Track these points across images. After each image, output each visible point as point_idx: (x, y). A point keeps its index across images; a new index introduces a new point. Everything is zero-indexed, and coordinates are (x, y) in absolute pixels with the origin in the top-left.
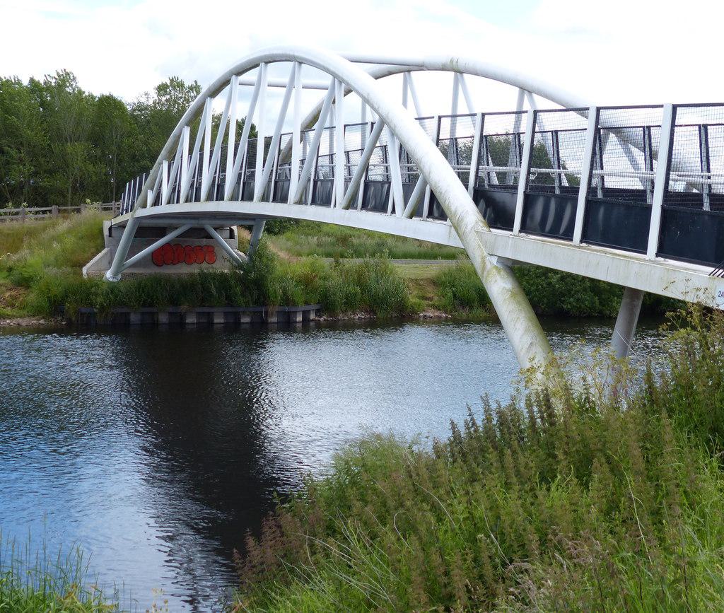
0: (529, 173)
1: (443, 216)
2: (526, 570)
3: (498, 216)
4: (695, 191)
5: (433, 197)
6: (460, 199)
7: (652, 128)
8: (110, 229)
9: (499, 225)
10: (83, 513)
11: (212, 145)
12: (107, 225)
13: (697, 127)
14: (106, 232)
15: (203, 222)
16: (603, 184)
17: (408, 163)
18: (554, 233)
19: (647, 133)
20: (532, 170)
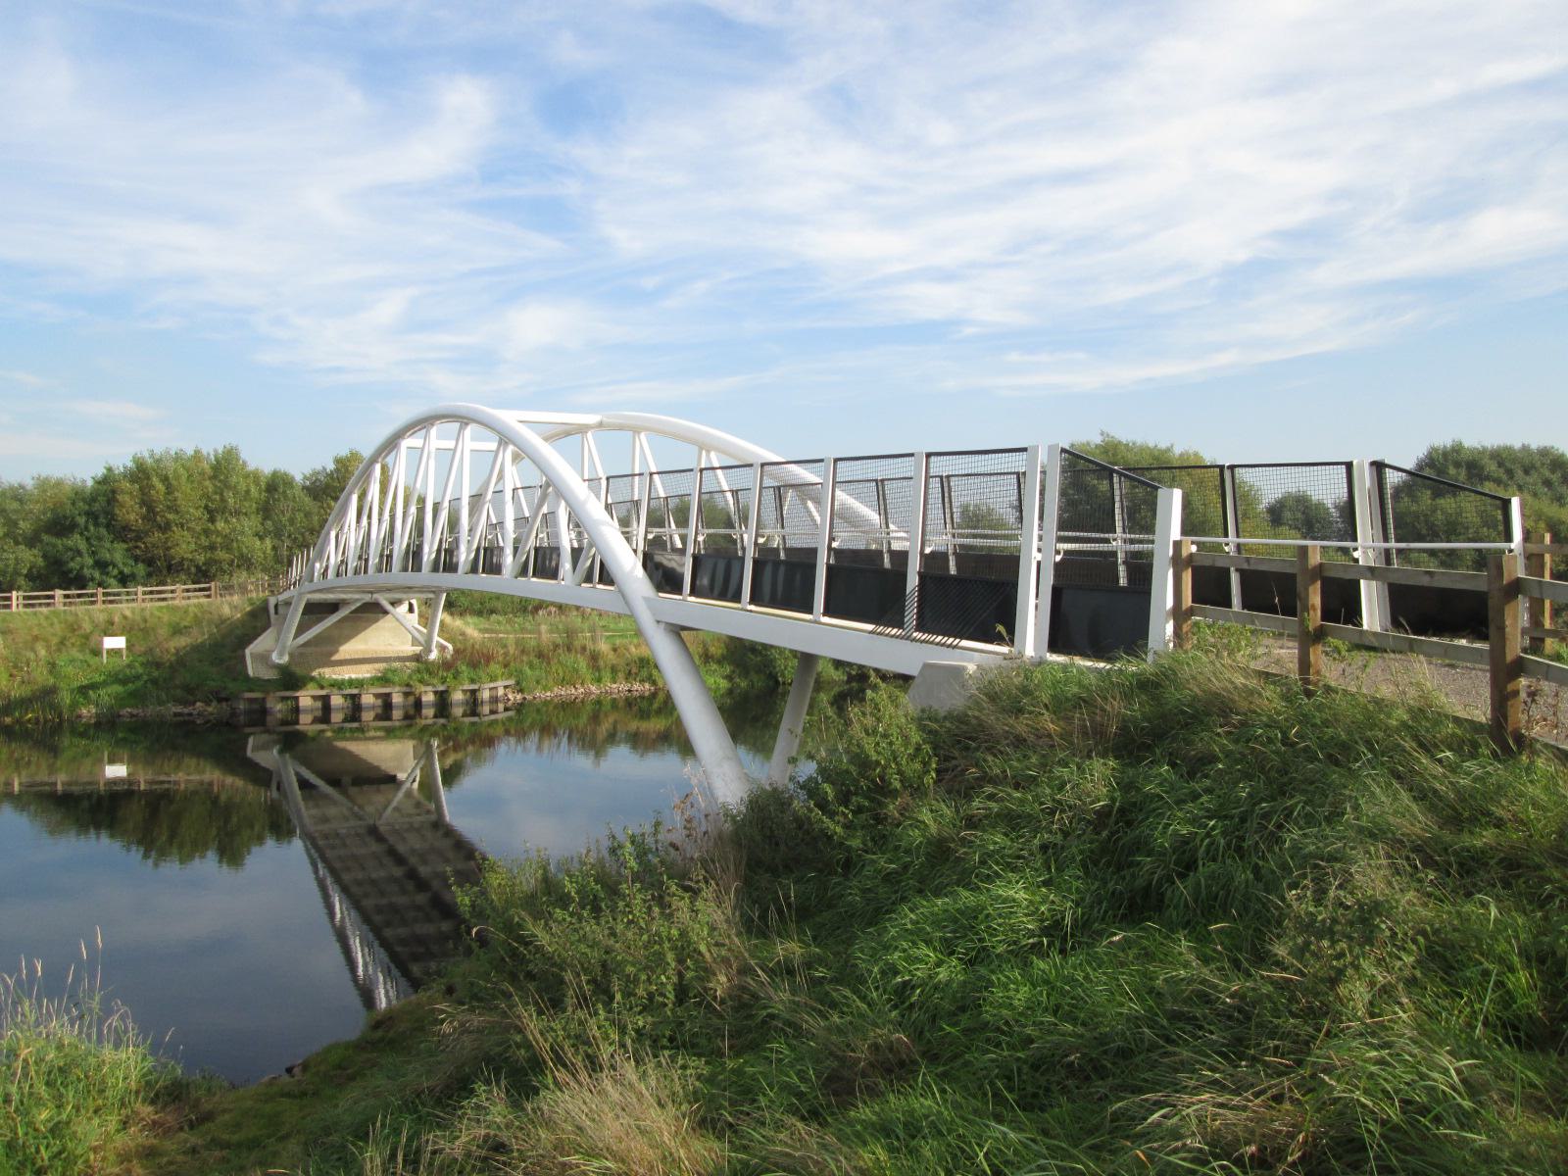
0: (646, 532)
1: (611, 582)
2: (48, 1084)
3: (665, 580)
4: (874, 547)
5: (602, 565)
6: (628, 563)
7: (953, 479)
8: (276, 606)
9: (668, 589)
10: (960, 1062)
11: (381, 514)
12: (272, 601)
13: (938, 479)
14: (272, 610)
15: (375, 596)
16: (785, 542)
17: (1238, 536)
18: (722, 597)
19: (946, 484)
20: (649, 529)
